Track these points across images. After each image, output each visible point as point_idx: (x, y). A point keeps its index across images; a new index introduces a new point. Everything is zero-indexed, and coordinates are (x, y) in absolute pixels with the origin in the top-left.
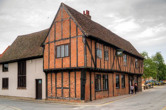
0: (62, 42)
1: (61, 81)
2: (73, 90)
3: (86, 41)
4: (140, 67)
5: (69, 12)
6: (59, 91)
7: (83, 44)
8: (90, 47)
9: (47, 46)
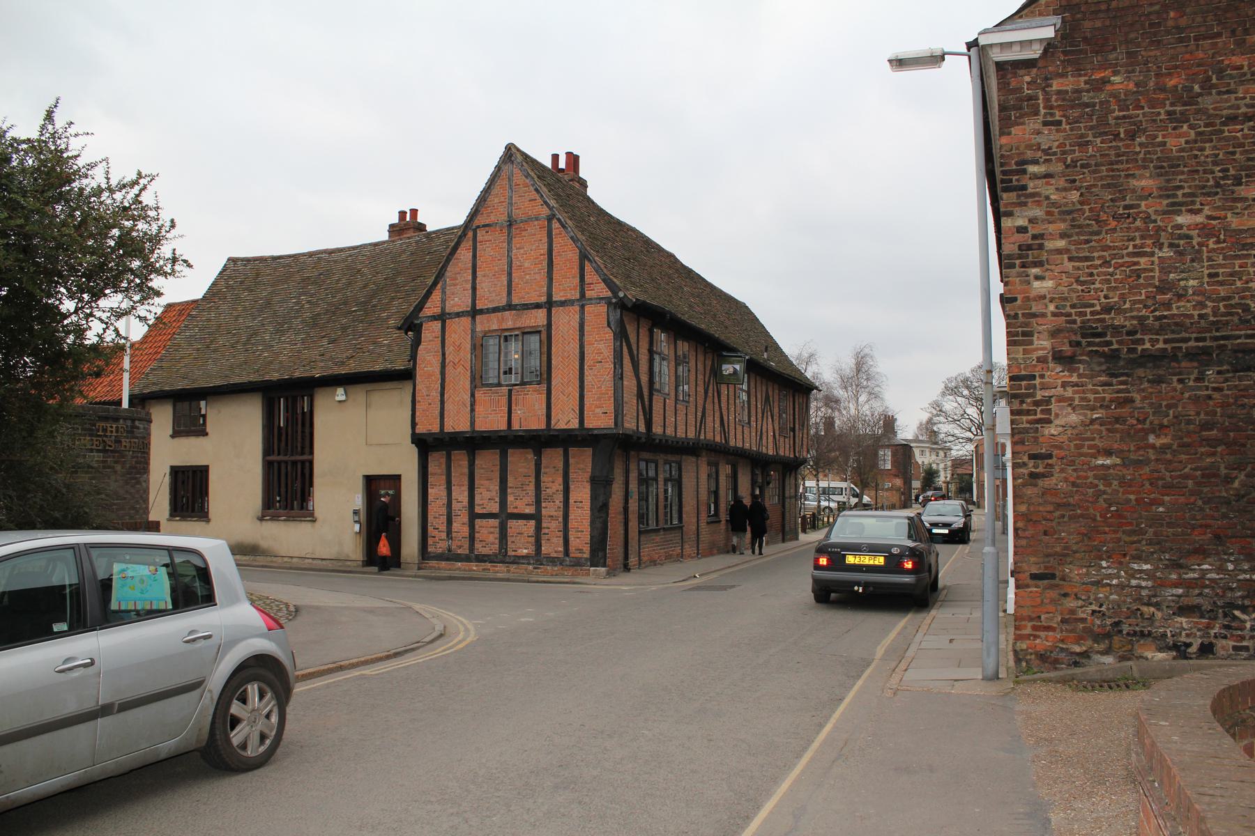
0: (510, 320)
1: (498, 488)
2: (552, 526)
3: (621, 324)
4: (797, 426)
5: (545, 189)
6: (488, 532)
7: (610, 336)
8: (634, 347)
9: (431, 331)
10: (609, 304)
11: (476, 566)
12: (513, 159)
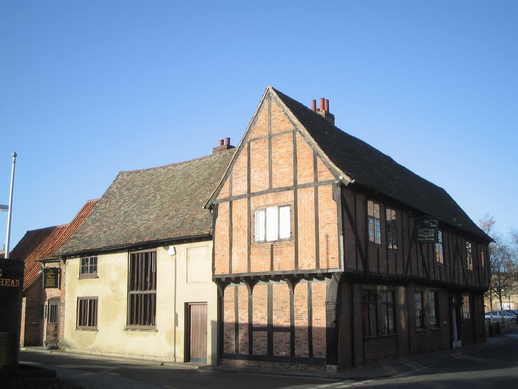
1: (267, 310)
9: (223, 209)
10: (333, 184)
11: (253, 363)
12: (271, 95)
